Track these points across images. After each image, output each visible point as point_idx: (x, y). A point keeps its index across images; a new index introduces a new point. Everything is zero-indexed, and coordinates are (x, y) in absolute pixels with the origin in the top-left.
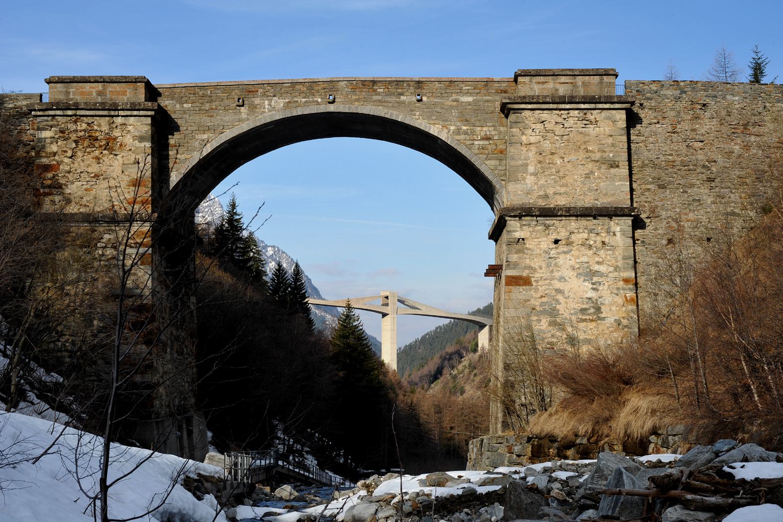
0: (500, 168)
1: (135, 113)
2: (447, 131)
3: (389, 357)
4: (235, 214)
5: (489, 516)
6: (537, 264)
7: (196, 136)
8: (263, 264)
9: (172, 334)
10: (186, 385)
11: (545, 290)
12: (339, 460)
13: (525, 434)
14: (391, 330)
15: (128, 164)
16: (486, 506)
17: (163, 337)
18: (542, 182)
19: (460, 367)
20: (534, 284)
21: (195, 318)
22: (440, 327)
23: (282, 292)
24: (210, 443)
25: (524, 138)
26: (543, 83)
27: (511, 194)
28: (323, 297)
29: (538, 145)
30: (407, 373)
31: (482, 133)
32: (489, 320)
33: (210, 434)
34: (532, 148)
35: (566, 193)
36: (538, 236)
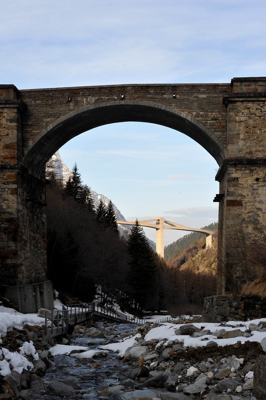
0: (223, 136)
1: (8, 106)
2: (191, 115)
3: (160, 251)
4: (77, 174)
5: (229, 367)
6: (246, 193)
7: (44, 119)
8: (93, 202)
9: (30, 235)
10: (40, 265)
11: (251, 209)
12: (132, 306)
13: (240, 295)
14: (161, 237)
15: (4, 136)
16: (225, 357)
17: (24, 237)
18: (248, 144)
19: (197, 256)
20: (244, 205)
21: (46, 227)
22: (186, 236)
23: (103, 216)
24: (57, 298)
25: (237, 118)
26: (249, 85)
27: (230, 151)
28: (126, 220)
29: (246, 122)
30: (169, 259)
31: (212, 116)
32: (212, 232)
33: (57, 293)
34: (242, 124)
35: (263, 150)
36: (246, 176)
